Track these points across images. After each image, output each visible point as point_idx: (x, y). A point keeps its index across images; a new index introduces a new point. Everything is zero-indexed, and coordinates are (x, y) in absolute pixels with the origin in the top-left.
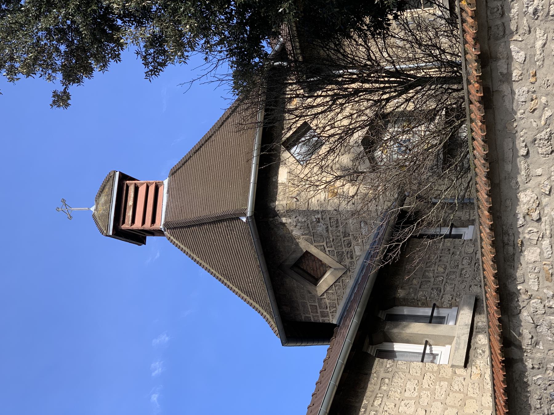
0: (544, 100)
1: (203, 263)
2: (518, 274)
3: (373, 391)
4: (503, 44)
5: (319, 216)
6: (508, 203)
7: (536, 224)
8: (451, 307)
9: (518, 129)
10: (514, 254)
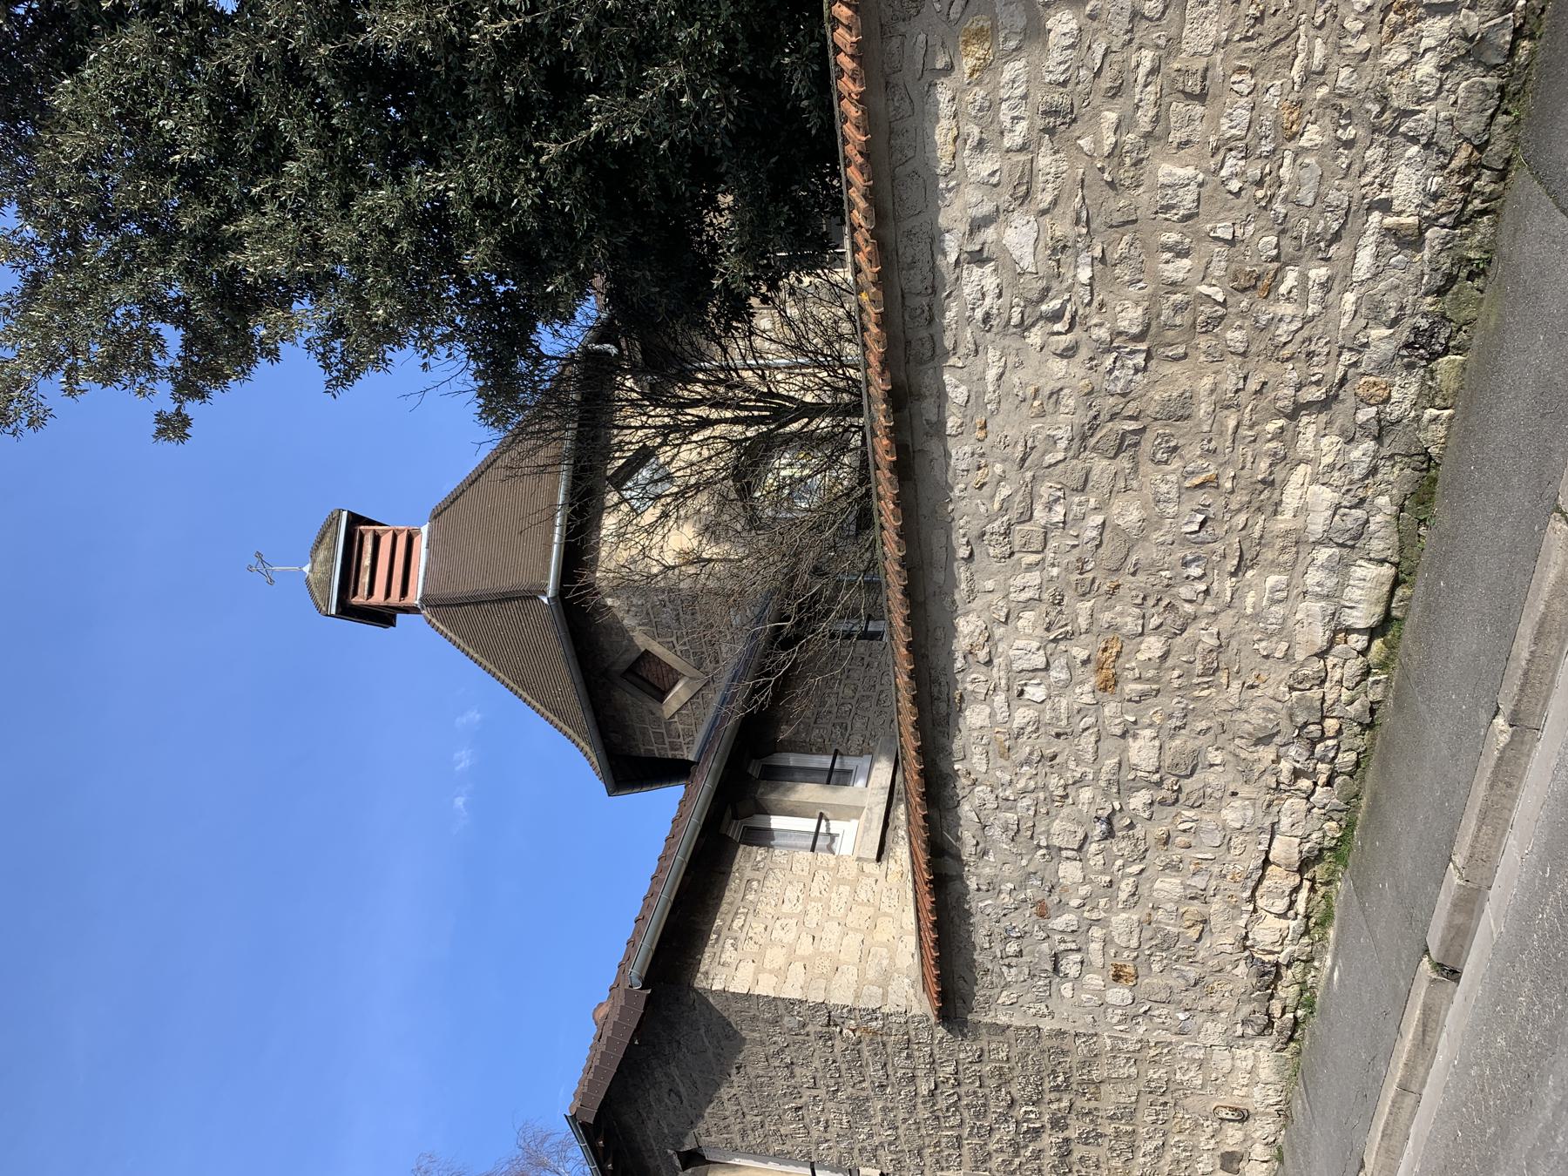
0: (998, 468)
1: (485, 662)
2: (954, 747)
3: (731, 904)
5: (665, 597)
6: (939, 633)
7: (984, 669)
8: (861, 754)
9: (956, 515)
10: (948, 715)
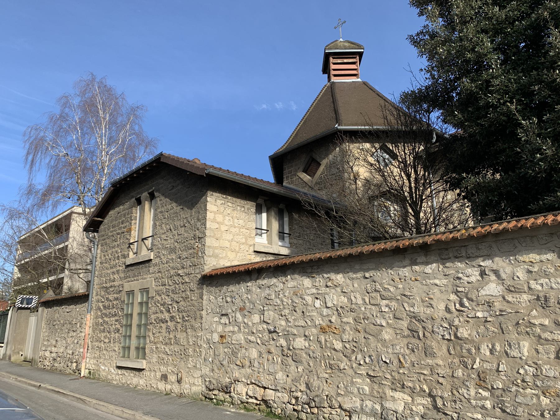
1: (312, 107)
2: (296, 275)
3: (236, 202)
4: (436, 259)
6: (336, 268)
7: (325, 285)
8: (290, 243)
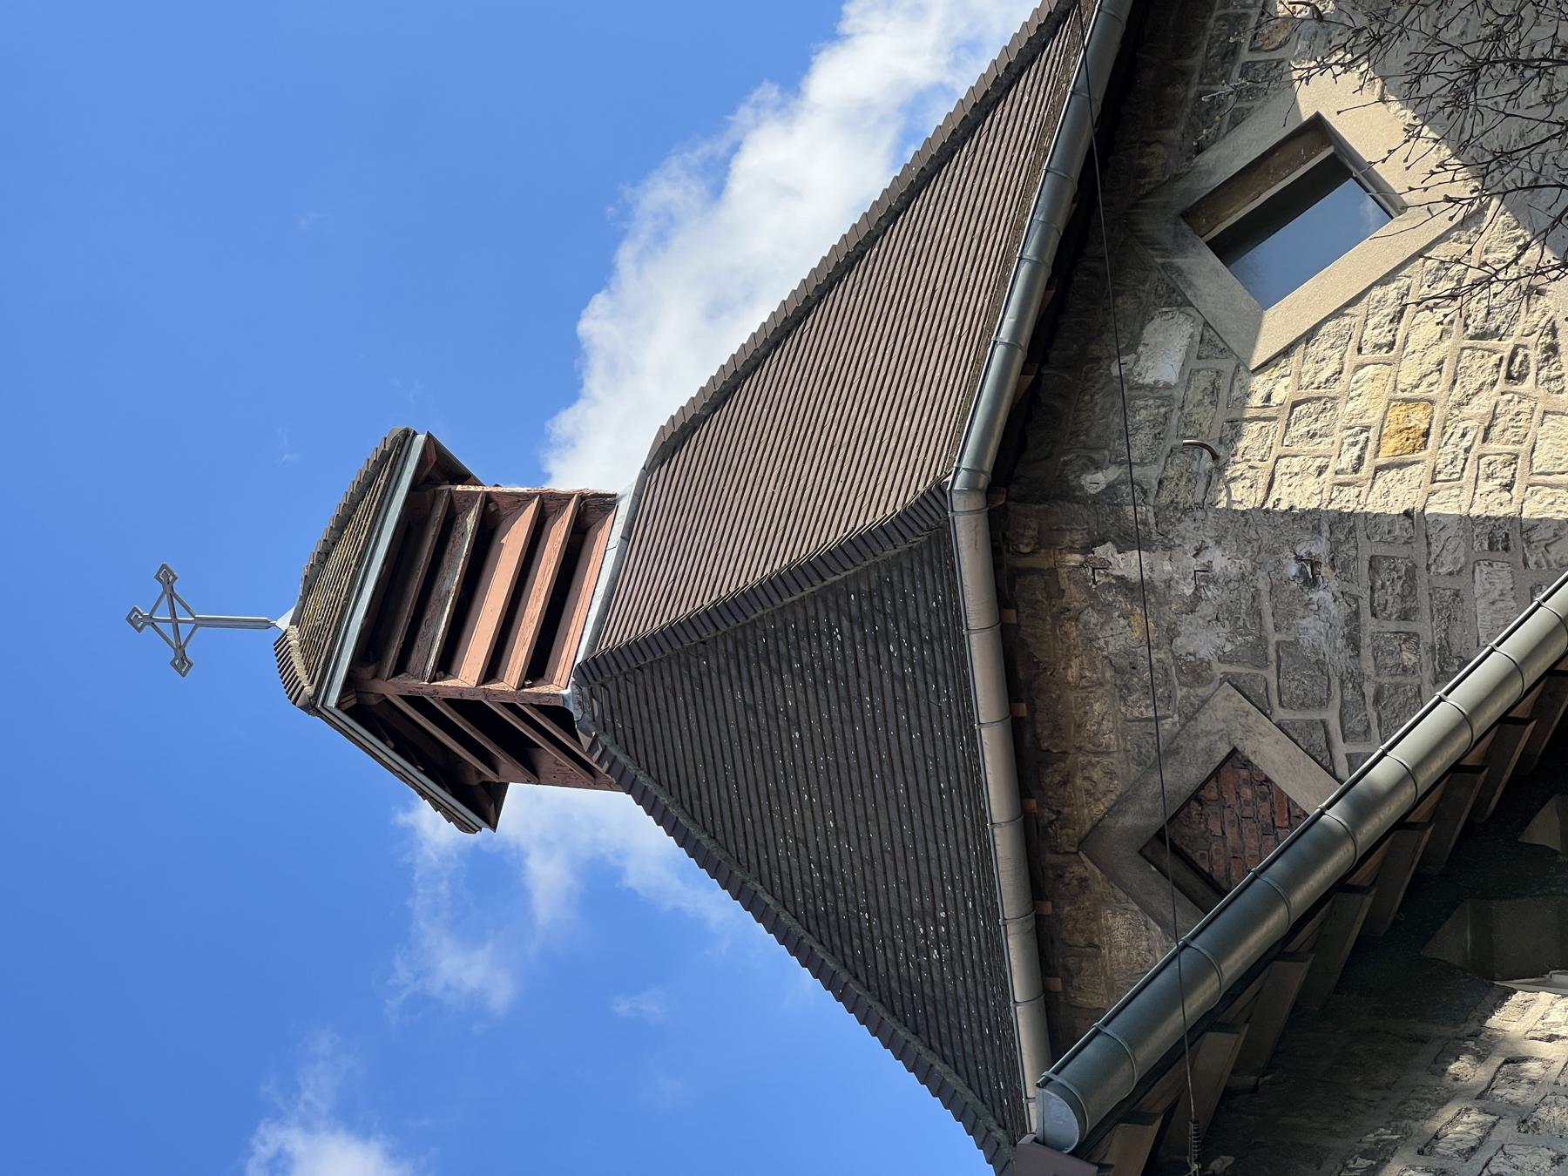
5: (1320, 549)
